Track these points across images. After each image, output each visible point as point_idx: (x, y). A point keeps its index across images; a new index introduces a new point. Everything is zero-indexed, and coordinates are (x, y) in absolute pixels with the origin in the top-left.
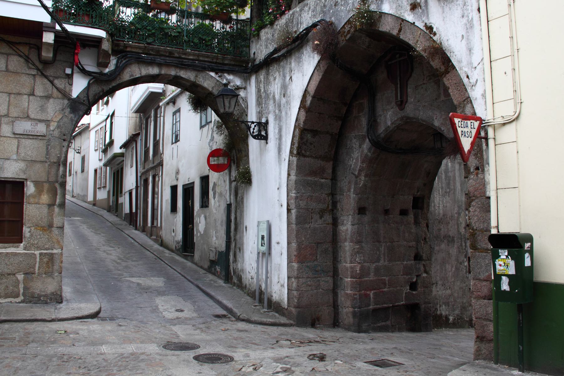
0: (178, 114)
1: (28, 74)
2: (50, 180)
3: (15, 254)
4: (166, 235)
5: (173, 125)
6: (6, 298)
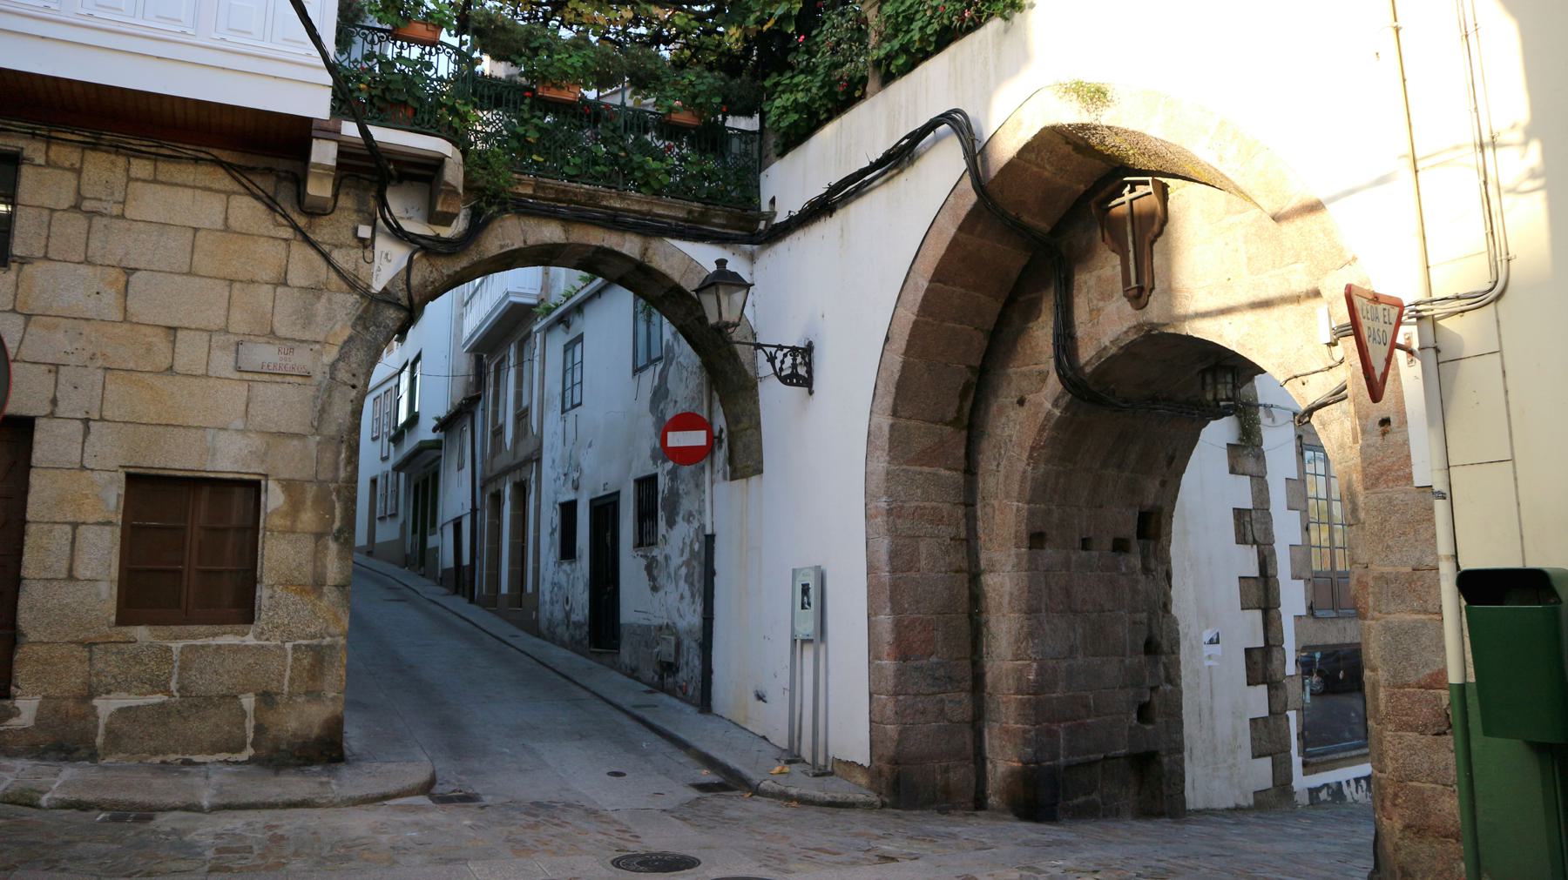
0: (579, 347)
2: (321, 477)
3: (235, 650)
4: (550, 609)
5: (565, 372)
6: (214, 753)
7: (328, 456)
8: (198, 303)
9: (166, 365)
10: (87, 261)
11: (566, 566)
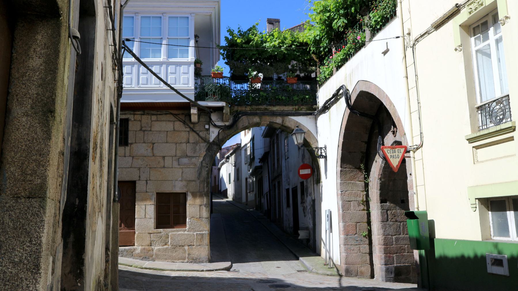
9: (163, 166)
10: (144, 142)
11: (288, 209)
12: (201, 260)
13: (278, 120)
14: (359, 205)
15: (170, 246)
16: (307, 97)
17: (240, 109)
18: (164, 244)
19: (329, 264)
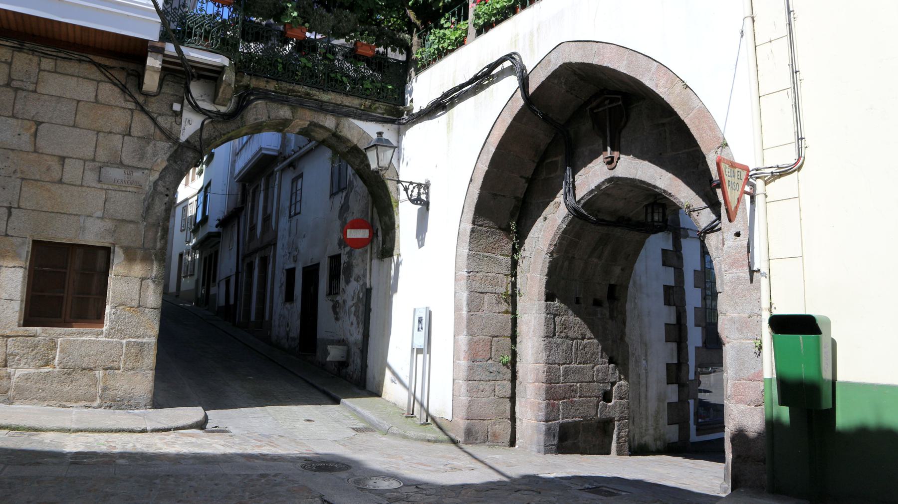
0: (300, 181)
1: (125, 108)
2: (146, 246)
7: (151, 234)
8: (79, 144)
9: (58, 178)
10: (13, 116)
11: (288, 305)
12: (133, 402)
13: (329, 122)
14: (499, 303)
15: (58, 369)
16: (390, 87)
17: (254, 83)
18: (41, 362)
19: (419, 414)
